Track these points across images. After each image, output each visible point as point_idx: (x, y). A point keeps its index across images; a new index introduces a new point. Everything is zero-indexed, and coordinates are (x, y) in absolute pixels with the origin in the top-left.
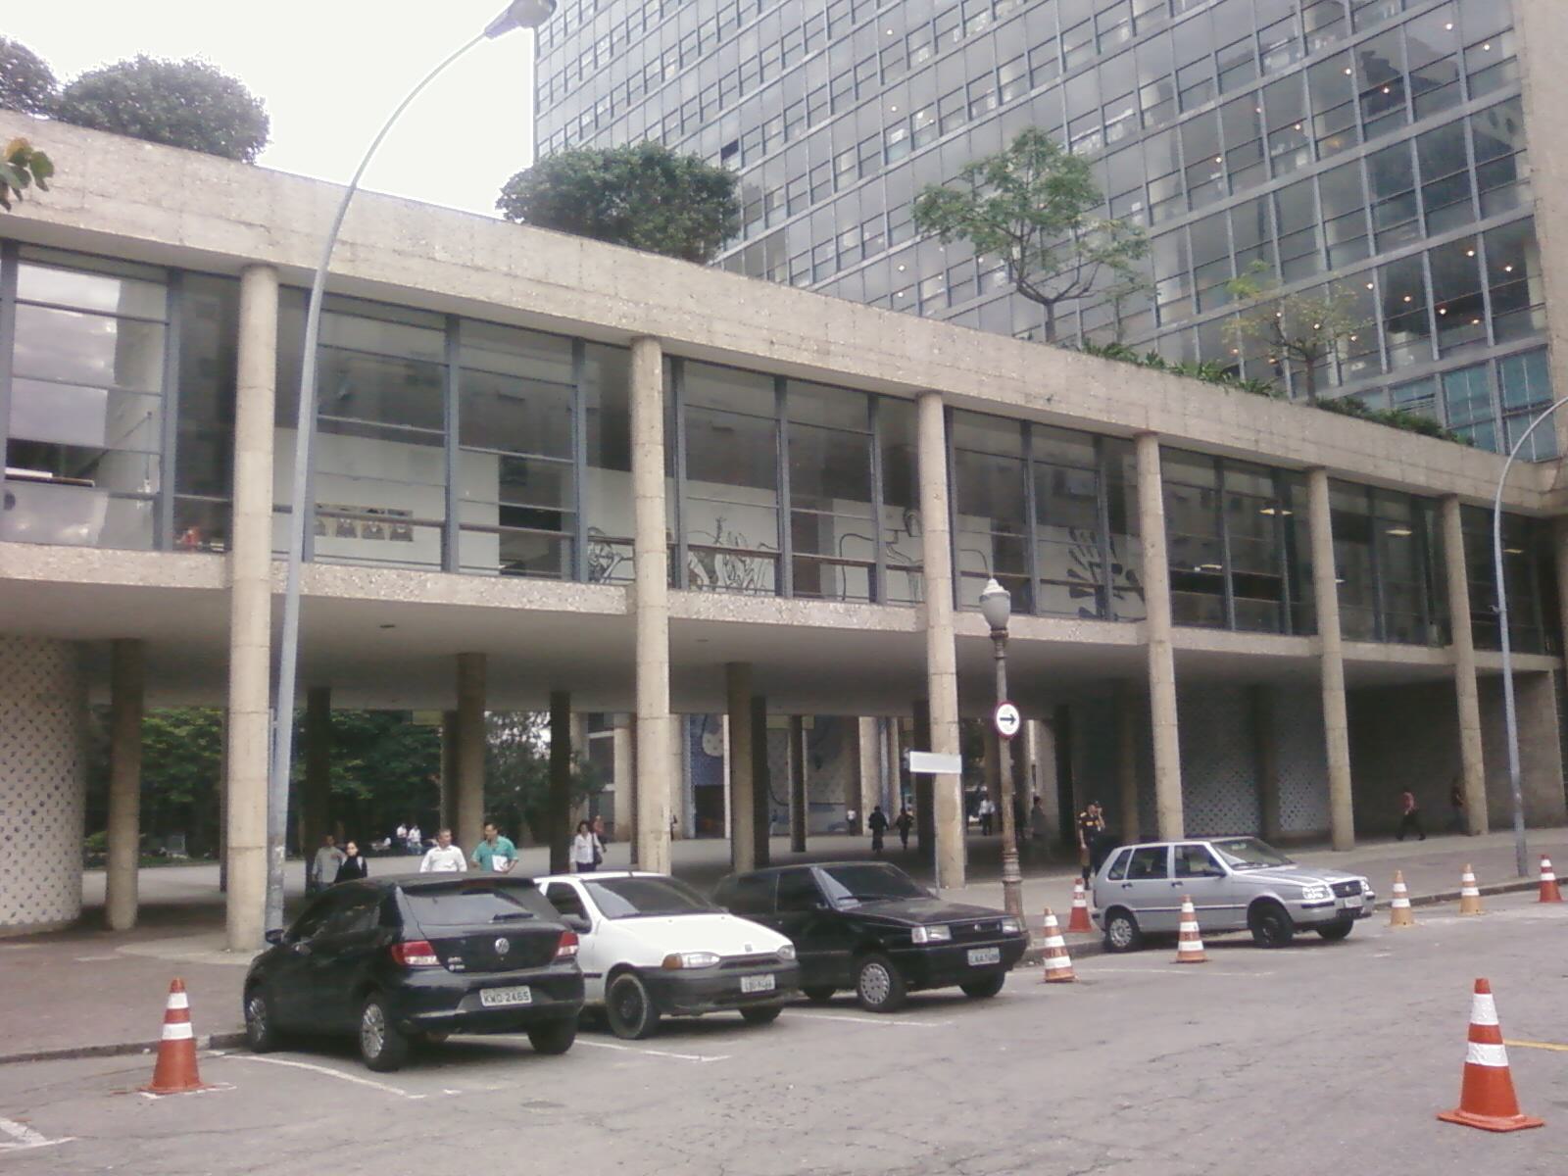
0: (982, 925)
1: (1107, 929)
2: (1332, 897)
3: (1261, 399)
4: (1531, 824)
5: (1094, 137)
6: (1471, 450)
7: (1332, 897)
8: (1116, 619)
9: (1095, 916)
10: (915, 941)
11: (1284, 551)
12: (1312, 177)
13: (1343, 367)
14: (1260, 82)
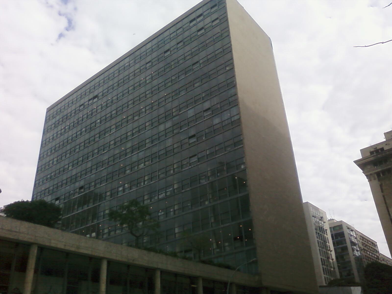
5: (164, 194)
14: (199, 185)
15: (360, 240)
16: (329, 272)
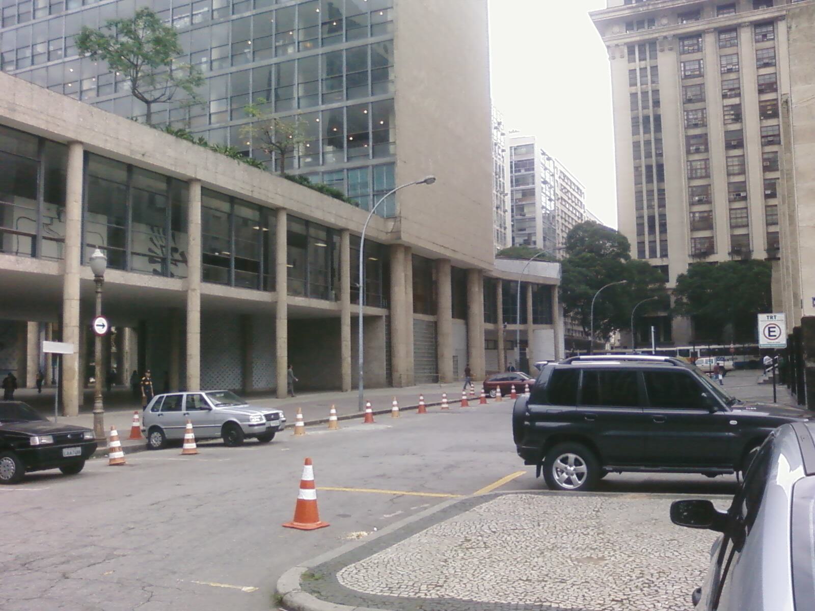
0: (72, 435)
1: (149, 438)
2: (264, 421)
3: (256, 169)
4: (365, 387)
5: (186, 19)
6: (357, 208)
7: (264, 421)
8: (172, 276)
9: (144, 431)
10: (32, 444)
11: (262, 249)
12: (295, 60)
13: (301, 159)
15: (558, 179)
16: (644, 251)
